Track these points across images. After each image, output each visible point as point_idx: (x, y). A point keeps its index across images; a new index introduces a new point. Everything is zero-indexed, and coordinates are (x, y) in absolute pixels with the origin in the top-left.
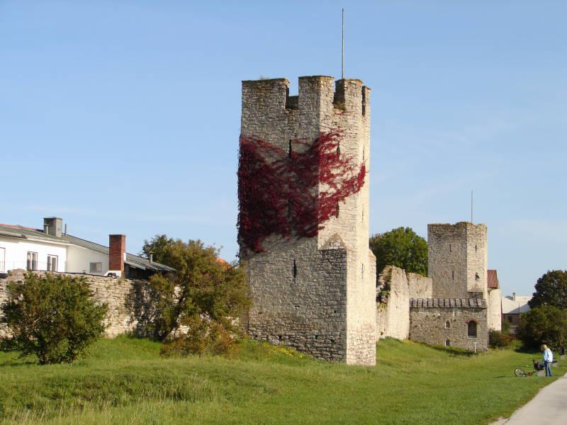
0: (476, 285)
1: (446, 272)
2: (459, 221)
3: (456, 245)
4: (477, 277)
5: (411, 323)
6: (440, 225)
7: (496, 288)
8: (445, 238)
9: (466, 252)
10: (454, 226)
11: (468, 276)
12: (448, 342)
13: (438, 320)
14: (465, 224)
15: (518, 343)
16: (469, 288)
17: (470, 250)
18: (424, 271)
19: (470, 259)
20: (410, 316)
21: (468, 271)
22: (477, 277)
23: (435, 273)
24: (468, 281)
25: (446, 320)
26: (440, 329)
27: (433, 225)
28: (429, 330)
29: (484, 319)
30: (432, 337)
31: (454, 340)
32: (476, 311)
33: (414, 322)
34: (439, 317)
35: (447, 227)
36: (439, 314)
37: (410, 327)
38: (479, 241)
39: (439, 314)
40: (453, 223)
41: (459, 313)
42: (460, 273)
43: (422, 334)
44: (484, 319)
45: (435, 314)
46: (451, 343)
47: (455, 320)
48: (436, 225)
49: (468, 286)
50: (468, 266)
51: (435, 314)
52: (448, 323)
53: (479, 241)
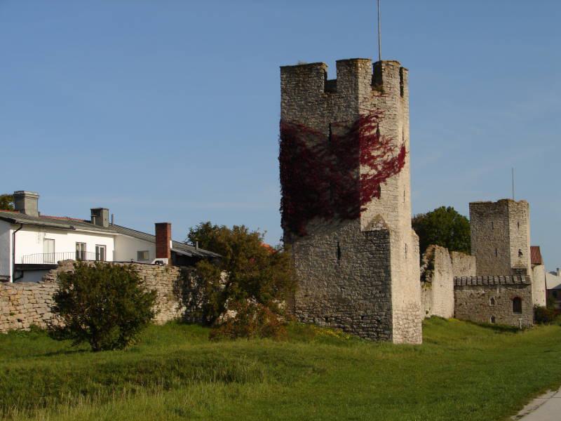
2: (501, 199)
3: (499, 223)
4: (520, 253)
5: (456, 301)
6: (482, 203)
7: (539, 264)
8: (487, 216)
9: (508, 229)
12: (493, 319)
14: (507, 200)
16: (513, 265)
17: (512, 227)
18: (467, 249)
19: (513, 236)
20: (455, 294)
22: (520, 253)
24: (512, 258)
25: (491, 298)
26: (485, 306)
27: (474, 204)
28: (474, 308)
31: (499, 317)
32: (520, 288)
33: (458, 300)
34: (483, 295)
35: (488, 204)
38: (521, 218)
39: (483, 292)
40: (494, 200)
41: (503, 290)
42: (503, 250)
46: (496, 320)
47: (500, 297)
48: (478, 204)
49: (512, 263)
50: (511, 243)
52: (492, 300)
53: (521, 218)
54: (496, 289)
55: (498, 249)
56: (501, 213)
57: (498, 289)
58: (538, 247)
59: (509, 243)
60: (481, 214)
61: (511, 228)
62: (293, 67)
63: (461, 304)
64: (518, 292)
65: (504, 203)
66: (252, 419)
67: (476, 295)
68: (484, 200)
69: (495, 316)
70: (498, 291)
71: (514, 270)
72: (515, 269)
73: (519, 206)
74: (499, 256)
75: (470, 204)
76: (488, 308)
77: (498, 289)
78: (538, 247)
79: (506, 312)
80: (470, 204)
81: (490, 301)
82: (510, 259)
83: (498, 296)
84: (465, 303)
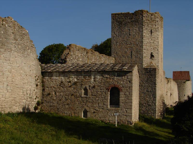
0: (151, 62)
1: (126, 52)
3: (134, 30)
4: (152, 56)
5: (43, 90)
6: (121, 14)
7: (189, 80)
10: (133, 14)
11: (144, 55)
12: (85, 113)
13: (74, 86)
14: (142, 11)
15: (43, 89)
16: (145, 65)
17: (146, 33)
19: (146, 41)
21: (144, 51)
22: (152, 56)
23: (116, 54)
24: (144, 59)
25: (84, 87)
26: (76, 97)
27: (115, 14)
29: (129, 85)
30: (67, 106)
31: (92, 110)
34: (75, 83)
35: (127, 15)
36: (76, 80)
37: (43, 95)
38: (154, 26)
39: (76, 80)
40: (132, 11)
41: (99, 77)
42: (137, 52)
43: (55, 104)
44: (129, 85)
45: (71, 79)
46: (89, 114)
47: (94, 87)
48: (118, 14)
49: (144, 63)
51: (71, 79)
52: (86, 89)
53: (154, 26)
54: (90, 76)
55: (133, 52)
56: (137, 21)
57: (93, 77)
58: (189, 72)
59: (142, 46)
60: (120, 23)
61: (144, 34)
62: (189, 74)
63: (49, 94)
64: (116, 81)
65: (140, 13)
66: (53, 143)
67: (66, 84)
68: (124, 12)
69: (88, 109)
70: (92, 80)
71: (146, 69)
72: (147, 69)
73: (153, 17)
74: (133, 57)
75: (112, 14)
76: (80, 99)
77: (93, 77)
78: (189, 72)
79: (101, 105)
80: (112, 14)
81: (83, 91)
82: (142, 60)
83: (92, 86)
84: (54, 93)
